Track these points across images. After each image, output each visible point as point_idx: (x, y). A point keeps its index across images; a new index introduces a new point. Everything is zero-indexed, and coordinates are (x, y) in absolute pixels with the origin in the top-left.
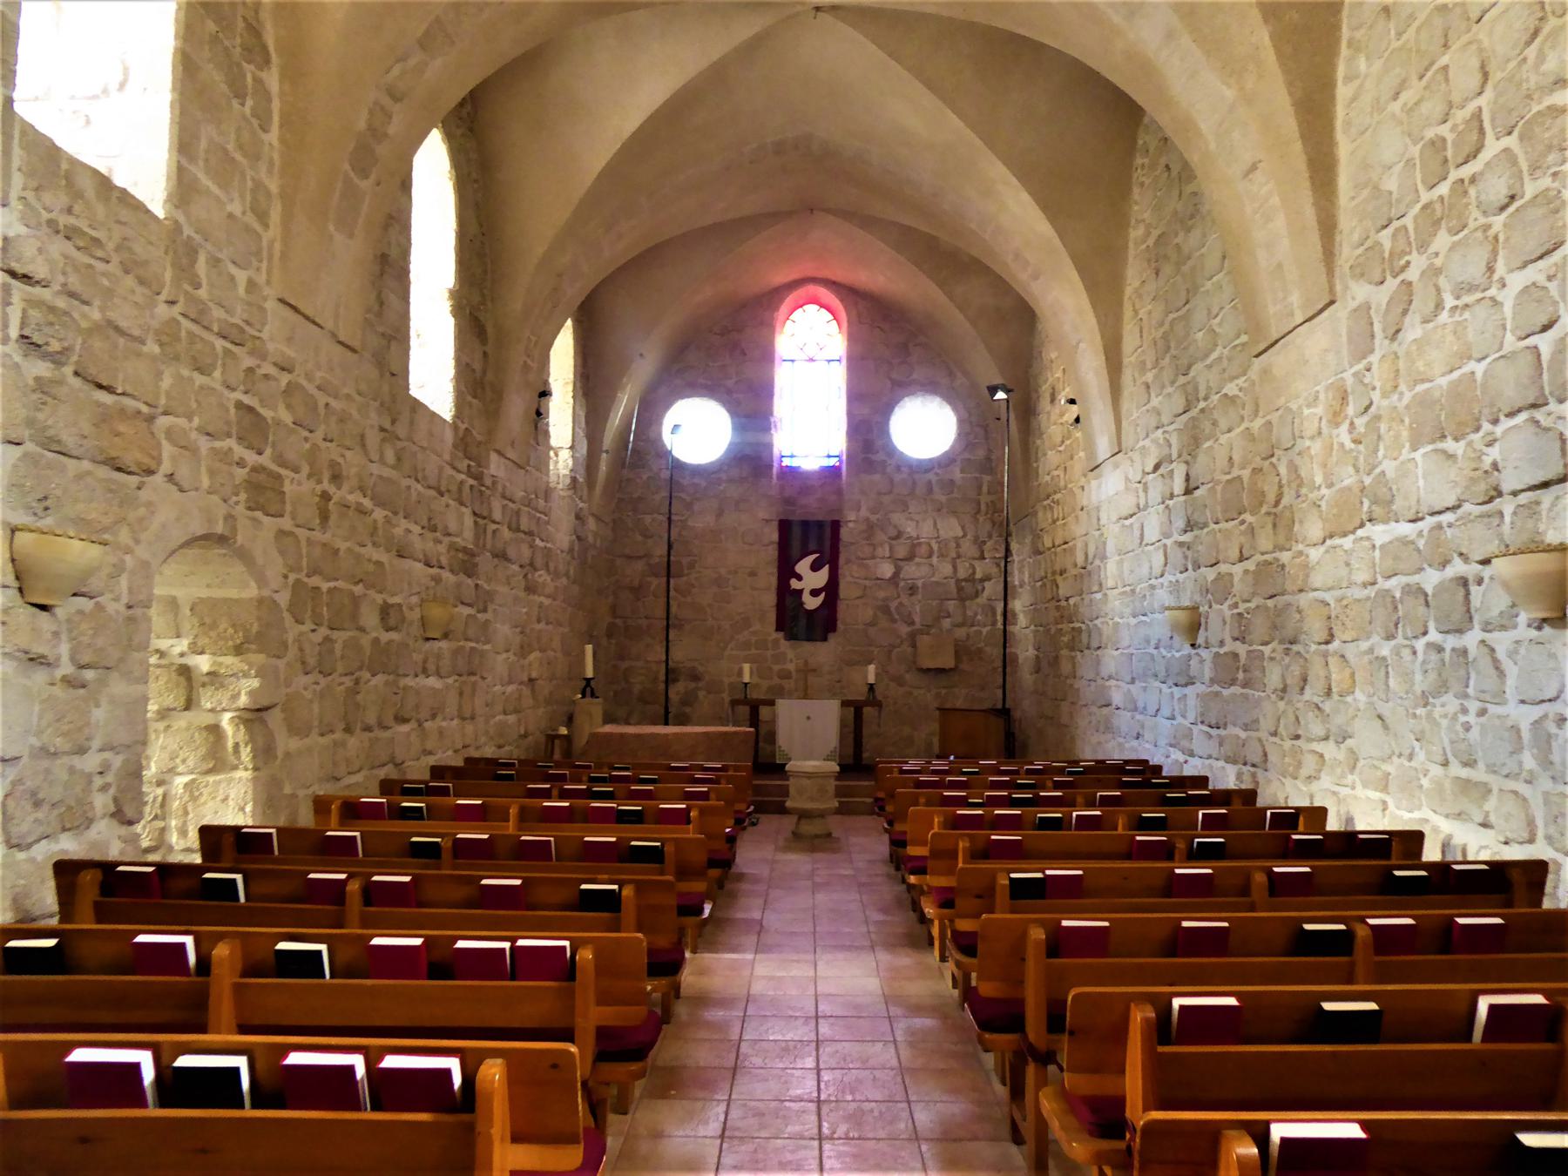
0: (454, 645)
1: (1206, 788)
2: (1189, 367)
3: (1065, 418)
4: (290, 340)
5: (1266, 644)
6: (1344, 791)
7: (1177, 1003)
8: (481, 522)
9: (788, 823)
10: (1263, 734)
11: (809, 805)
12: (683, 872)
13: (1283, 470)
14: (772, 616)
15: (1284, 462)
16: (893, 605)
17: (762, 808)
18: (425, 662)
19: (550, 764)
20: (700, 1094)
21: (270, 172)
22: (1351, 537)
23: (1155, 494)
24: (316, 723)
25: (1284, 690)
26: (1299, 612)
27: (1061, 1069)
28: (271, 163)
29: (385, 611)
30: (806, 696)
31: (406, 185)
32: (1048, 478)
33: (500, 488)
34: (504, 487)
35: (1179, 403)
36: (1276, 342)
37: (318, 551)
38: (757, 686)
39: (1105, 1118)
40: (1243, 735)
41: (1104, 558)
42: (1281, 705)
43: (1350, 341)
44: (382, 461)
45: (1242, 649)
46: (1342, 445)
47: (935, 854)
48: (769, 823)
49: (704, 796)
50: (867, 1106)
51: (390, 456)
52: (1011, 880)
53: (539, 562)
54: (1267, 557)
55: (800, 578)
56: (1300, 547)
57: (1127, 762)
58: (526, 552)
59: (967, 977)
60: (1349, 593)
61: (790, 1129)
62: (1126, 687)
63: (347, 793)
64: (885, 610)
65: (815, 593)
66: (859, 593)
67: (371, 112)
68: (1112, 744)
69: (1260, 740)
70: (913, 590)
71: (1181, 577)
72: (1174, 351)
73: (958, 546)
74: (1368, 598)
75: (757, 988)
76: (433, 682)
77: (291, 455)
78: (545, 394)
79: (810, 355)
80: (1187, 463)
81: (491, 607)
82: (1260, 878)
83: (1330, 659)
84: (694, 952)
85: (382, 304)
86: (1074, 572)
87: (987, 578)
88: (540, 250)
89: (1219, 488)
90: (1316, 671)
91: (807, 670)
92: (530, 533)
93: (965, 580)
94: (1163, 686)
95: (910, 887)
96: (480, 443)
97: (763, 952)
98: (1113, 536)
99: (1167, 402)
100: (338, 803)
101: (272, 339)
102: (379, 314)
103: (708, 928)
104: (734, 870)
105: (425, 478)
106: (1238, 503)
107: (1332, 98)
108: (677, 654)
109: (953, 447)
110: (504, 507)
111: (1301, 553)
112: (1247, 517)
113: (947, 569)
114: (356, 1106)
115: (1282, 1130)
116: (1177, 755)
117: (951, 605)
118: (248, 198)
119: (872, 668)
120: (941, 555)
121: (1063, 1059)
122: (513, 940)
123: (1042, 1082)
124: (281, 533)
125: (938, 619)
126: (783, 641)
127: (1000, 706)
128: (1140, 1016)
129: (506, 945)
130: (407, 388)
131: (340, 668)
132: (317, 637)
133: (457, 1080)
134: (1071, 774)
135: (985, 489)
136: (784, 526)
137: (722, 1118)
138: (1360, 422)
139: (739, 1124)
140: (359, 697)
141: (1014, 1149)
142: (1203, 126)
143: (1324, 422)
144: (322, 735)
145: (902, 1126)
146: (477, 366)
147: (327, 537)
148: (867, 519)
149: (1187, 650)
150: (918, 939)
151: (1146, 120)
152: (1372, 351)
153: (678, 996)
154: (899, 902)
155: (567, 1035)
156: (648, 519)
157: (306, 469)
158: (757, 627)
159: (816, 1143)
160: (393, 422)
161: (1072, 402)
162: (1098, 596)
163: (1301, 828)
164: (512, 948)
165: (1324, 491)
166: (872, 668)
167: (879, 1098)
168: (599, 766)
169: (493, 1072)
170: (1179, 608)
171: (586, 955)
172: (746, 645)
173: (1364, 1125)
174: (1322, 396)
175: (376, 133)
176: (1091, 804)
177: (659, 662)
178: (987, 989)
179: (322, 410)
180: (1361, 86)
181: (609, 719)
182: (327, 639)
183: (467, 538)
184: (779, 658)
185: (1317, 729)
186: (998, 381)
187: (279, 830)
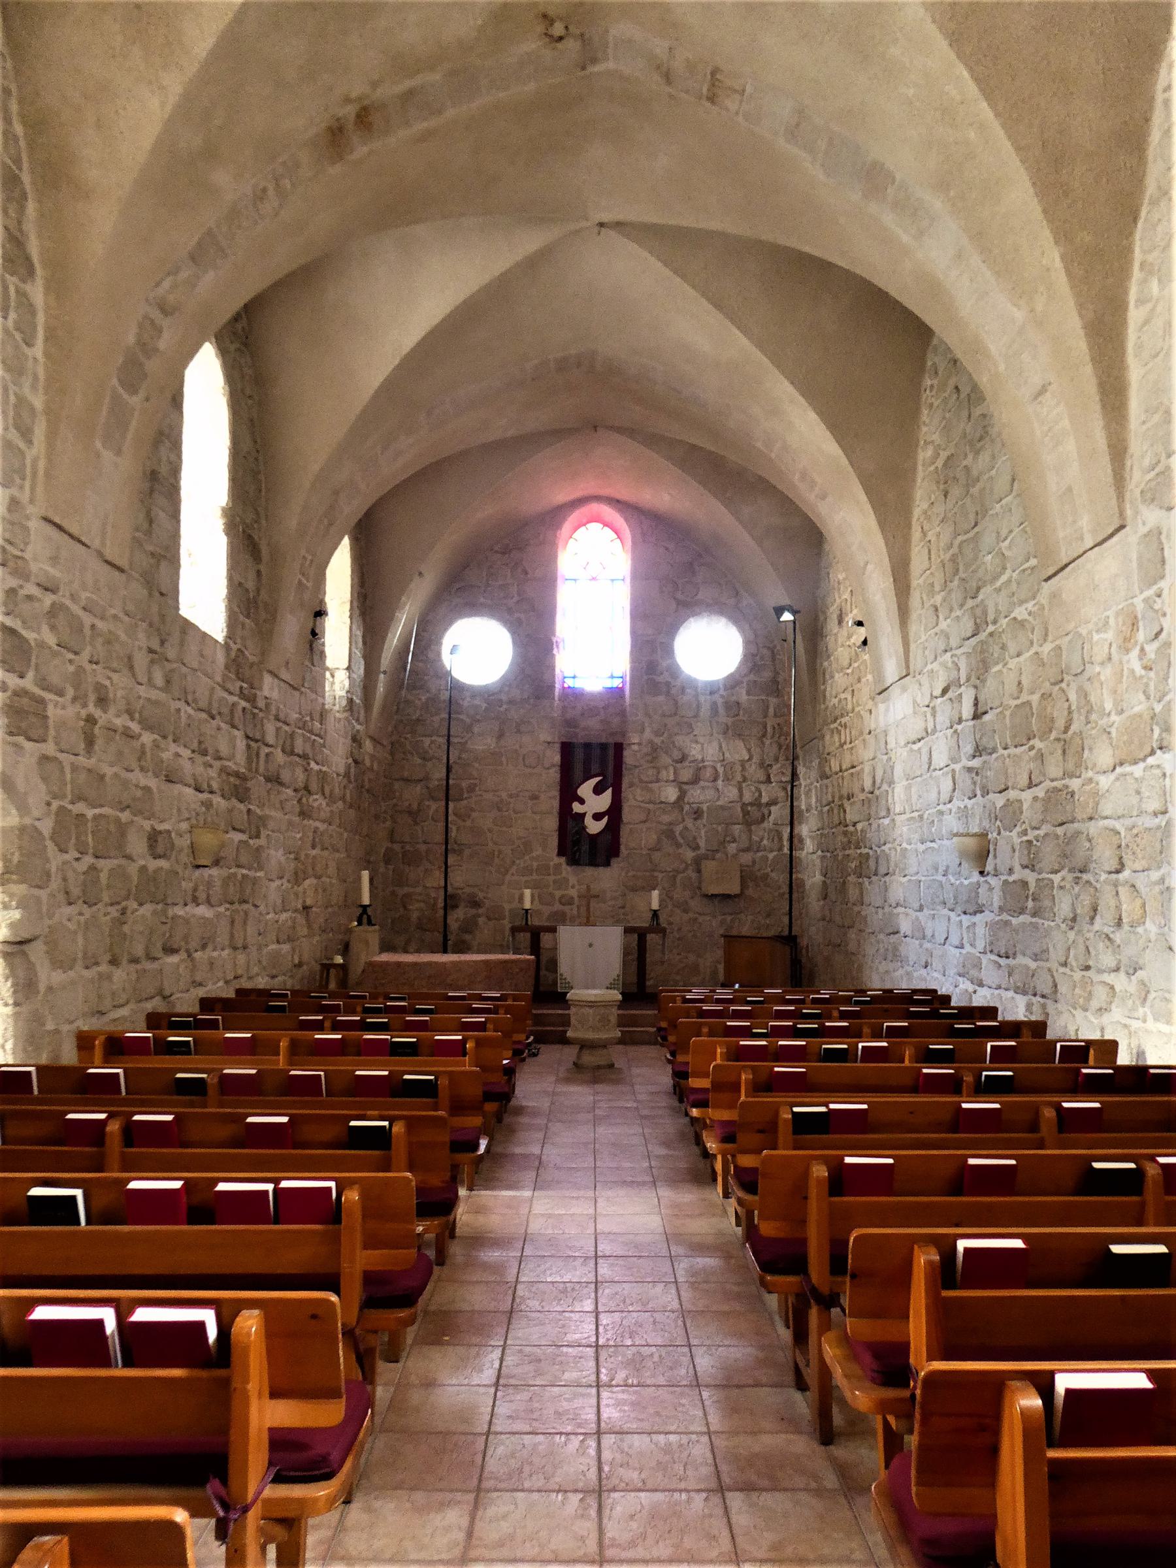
0: (224, 872)
1: (995, 1018)
2: (978, 589)
3: (852, 640)
4: (54, 560)
5: (1056, 872)
6: (1135, 1024)
7: (962, 1245)
8: (252, 744)
9: (569, 1054)
10: (1054, 965)
11: (590, 1035)
12: (458, 1107)
13: (1073, 697)
14: (554, 841)
15: (1074, 686)
16: (678, 829)
17: (543, 1039)
18: (195, 890)
19: (327, 992)
20: (475, 1340)
21: (34, 387)
22: (1142, 765)
23: (943, 719)
24: (80, 955)
25: (1074, 919)
26: (1090, 841)
27: (843, 1310)
28: (35, 377)
29: (153, 838)
30: (588, 923)
31: (177, 401)
32: (836, 701)
33: (274, 712)
34: (278, 709)
35: (968, 626)
36: (1066, 566)
37: (83, 777)
38: (538, 912)
39: (890, 1366)
40: (1033, 965)
41: (891, 783)
42: (1072, 935)
43: (1140, 566)
44: (150, 683)
45: (1031, 877)
46: (1133, 671)
47: (717, 1086)
48: (550, 1054)
49: (481, 1027)
50: (646, 1351)
51: (159, 680)
52: (794, 1114)
53: (314, 786)
54: (1055, 784)
55: (582, 802)
56: (1090, 774)
57: (915, 992)
58: (301, 776)
59: (750, 1214)
60: (1140, 821)
61: (567, 1376)
62: (914, 914)
63: (111, 1028)
64: (669, 834)
65: (597, 817)
66: (643, 817)
67: (141, 326)
68: (901, 972)
69: (1049, 970)
70: (698, 814)
71: (970, 803)
72: (964, 576)
73: (744, 769)
74: (1159, 827)
75: (535, 1226)
76: (203, 911)
77: (55, 679)
78: (320, 613)
79: (594, 579)
80: (976, 687)
81: (264, 833)
82: (1049, 1113)
83: (1120, 888)
84: (470, 1189)
85: (151, 522)
86: (862, 796)
87: (773, 802)
88: (315, 468)
89: (1008, 713)
90: (1107, 901)
91: (589, 897)
92: (305, 757)
93: (751, 804)
94: (952, 914)
95: (694, 1121)
96: (252, 665)
97: (541, 1189)
98: (902, 760)
99: (956, 625)
100: (102, 1038)
101: (35, 559)
102: (149, 533)
103: (484, 1166)
104: (514, 1102)
105: (195, 700)
106: (1027, 737)
107: (1124, 322)
108: (458, 879)
109: (738, 668)
110: (278, 729)
111: (1091, 780)
112: (1037, 743)
113: (732, 793)
114: (106, 1362)
115: (1067, 1380)
116: (966, 985)
117: (737, 829)
118: (11, 413)
119: (655, 894)
120: (727, 779)
121: (845, 1301)
122: (276, 1181)
123: (826, 1325)
124: (44, 759)
125: (723, 843)
126: (564, 866)
127: (786, 933)
128: (924, 1258)
129: (269, 1187)
130: (178, 608)
131: (106, 899)
132: (82, 866)
133: (212, 1333)
134: (857, 1003)
135: (771, 710)
136: (567, 749)
137: (497, 1365)
138: (1151, 649)
139: (518, 1371)
140: (126, 928)
141: (798, 1396)
142: (993, 348)
143: (1114, 646)
144: (87, 968)
145: (683, 1372)
146: (251, 585)
147: (91, 762)
148: (651, 742)
149: (976, 877)
150: (702, 1176)
151: (935, 341)
152: (1162, 577)
153: (452, 1236)
154: (682, 1136)
155: (331, 1283)
156: (427, 741)
157: (70, 692)
158: (538, 851)
159: (594, 1391)
160: (162, 642)
161: (860, 624)
162: (886, 821)
163: (1091, 1062)
164: (275, 1190)
165: (1114, 717)
166: (655, 894)
167: (659, 1341)
168: (374, 997)
169: (249, 1324)
170: (967, 835)
171: (353, 1196)
172: (528, 871)
173: (1151, 1374)
174: (1112, 621)
175: (146, 347)
176: (877, 1036)
177: (438, 888)
178: (767, 1229)
179: (87, 631)
180: (1153, 310)
181: (386, 947)
182: (92, 868)
183: (239, 762)
184: (562, 884)
185: (1108, 960)
186: (785, 601)
187: (40, 1069)
